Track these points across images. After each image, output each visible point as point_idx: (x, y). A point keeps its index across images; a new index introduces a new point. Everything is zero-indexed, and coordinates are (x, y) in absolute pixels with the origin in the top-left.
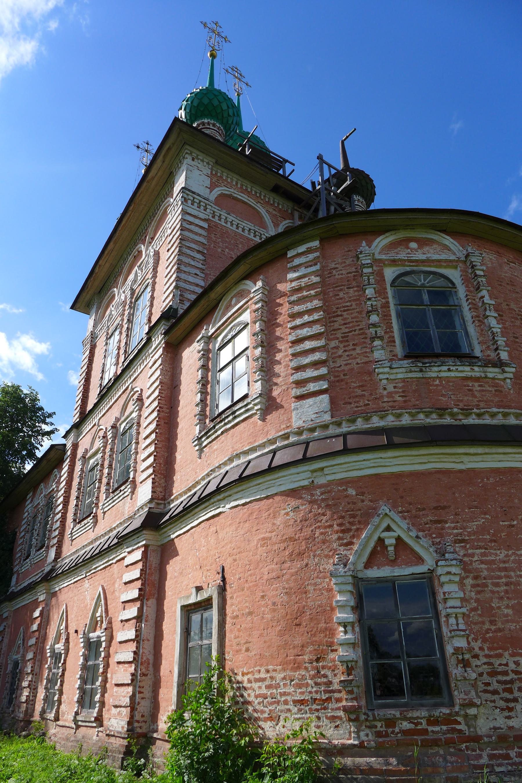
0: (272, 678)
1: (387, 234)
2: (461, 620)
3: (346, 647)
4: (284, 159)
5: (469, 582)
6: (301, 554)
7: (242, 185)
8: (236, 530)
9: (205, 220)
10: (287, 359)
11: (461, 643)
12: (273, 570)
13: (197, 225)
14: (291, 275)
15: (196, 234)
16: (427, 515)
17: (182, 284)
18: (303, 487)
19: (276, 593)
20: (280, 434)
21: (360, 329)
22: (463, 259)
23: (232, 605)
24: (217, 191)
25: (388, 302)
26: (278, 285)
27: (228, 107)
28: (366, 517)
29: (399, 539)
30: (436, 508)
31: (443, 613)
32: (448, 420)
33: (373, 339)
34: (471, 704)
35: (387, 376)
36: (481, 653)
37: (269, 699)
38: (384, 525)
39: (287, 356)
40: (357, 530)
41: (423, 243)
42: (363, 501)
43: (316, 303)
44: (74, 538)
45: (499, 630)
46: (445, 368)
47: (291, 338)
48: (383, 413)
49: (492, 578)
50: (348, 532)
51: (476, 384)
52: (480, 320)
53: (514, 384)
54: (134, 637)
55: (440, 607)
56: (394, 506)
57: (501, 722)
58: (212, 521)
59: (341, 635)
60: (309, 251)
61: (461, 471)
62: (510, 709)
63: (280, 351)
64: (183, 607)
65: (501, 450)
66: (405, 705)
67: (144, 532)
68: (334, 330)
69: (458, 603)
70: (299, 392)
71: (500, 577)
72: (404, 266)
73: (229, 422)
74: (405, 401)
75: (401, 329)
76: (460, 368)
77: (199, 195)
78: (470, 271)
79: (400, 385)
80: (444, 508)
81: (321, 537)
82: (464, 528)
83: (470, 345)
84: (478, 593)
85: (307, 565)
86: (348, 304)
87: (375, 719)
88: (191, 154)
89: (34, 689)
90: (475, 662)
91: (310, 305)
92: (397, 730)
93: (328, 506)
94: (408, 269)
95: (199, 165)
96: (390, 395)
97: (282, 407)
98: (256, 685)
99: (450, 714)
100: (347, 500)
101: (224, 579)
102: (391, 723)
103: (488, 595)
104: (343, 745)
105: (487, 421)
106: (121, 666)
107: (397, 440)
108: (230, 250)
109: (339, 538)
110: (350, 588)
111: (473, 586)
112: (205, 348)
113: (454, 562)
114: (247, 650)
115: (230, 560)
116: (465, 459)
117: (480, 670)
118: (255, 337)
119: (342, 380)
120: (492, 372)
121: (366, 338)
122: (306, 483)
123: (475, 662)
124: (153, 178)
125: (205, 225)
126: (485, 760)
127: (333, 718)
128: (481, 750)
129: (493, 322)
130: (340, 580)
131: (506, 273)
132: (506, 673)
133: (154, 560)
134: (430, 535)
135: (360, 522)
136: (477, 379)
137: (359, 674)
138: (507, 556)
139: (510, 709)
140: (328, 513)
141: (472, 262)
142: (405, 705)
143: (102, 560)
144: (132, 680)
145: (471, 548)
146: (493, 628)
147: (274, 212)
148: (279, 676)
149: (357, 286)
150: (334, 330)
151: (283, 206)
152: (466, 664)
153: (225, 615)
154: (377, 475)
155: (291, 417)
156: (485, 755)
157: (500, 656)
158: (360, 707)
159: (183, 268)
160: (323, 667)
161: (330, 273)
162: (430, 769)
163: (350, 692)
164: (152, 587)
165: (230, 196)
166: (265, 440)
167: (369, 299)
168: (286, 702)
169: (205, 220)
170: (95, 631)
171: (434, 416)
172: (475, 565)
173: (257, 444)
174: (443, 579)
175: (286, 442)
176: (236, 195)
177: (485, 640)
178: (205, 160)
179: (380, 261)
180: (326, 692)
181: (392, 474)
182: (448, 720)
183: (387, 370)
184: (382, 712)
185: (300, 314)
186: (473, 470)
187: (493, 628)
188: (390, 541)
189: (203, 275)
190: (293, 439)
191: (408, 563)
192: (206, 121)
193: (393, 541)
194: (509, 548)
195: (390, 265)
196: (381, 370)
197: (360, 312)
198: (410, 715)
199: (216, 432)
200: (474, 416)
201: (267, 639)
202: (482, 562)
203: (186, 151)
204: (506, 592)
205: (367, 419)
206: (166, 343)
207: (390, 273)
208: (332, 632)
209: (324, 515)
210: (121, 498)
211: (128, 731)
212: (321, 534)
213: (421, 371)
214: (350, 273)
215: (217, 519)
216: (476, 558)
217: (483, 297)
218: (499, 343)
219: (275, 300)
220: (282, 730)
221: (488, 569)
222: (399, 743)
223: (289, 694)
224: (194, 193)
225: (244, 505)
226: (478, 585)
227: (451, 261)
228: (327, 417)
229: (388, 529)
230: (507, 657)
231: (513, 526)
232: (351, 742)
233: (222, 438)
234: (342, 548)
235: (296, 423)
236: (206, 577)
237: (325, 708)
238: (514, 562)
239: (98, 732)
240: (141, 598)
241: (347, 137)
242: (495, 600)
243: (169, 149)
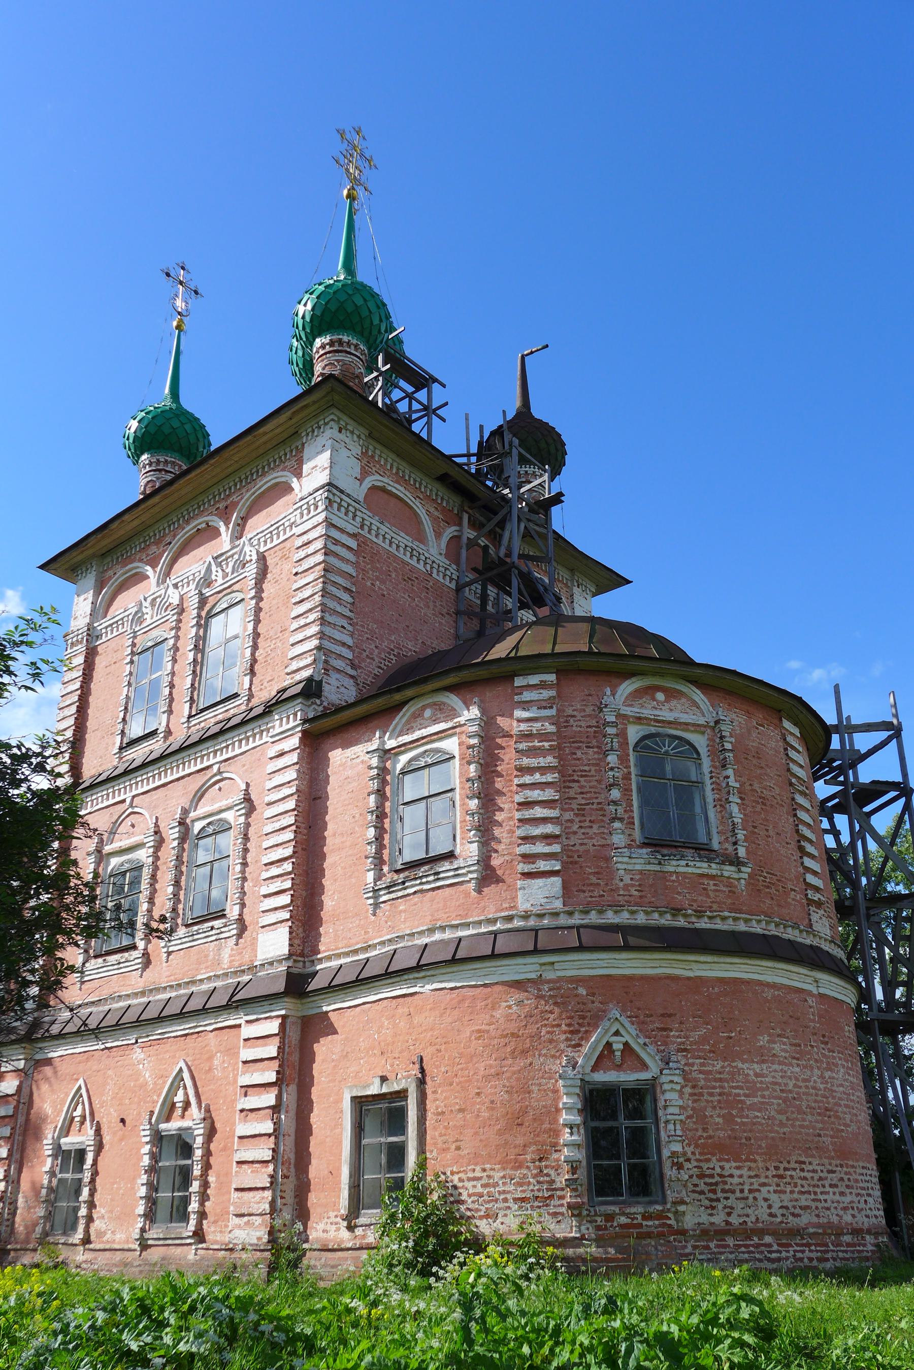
0: (489, 1177)
1: (633, 679)
2: (678, 1127)
3: (571, 1148)
4: (431, 377)
5: (688, 1090)
6: (524, 1052)
7: (398, 469)
8: (441, 1016)
9: (354, 536)
10: (511, 823)
11: (677, 1147)
12: (491, 1066)
13: (344, 545)
14: (519, 713)
15: (342, 559)
16: (654, 1022)
17: (327, 644)
18: (529, 980)
19: (496, 1091)
20: (503, 914)
21: (599, 803)
22: (712, 724)
23: (436, 1100)
24: (368, 482)
25: (630, 773)
26: (499, 718)
27: (365, 300)
28: (595, 1019)
29: (626, 1044)
30: (663, 1015)
31: (663, 1119)
32: (681, 922)
33: (613, 820)
34: (683, 1202)
35: (625, 866)
36: (693, 1158)
37: (486, 1198)
38: (613, 1030)
39: (511, 818)
40: (586, 1032)
41: (672, 694)
42: (593, 1002)
43: (550, 760)
44: (86, 979)
45: (710, 1137)
46: (683, 863)
47: (519, 798)
48: (617, 907)
49: (708, 1087)
50: (577, 1035)
51: (712, 883)
52: (722, 804)
53: (748, 884)
54: (271, 1131)
55: (660, 1113)
56: (623, 1011)
57: (705, 1218)
58: (401, 1000)
59: (566, 1136)
60: (543, 685)
61: (689, 978)
62: (713, 1208)
63: (501, 809)
64: (354, 1099)
65: (729, 960)
66: (623, 1202)
67: (286, 999)
68: (569, 798)
69: (677, 1111)
70: (527, 868)
71: (714, 1088)
72: (649, 725)
73: (428, 882)
74: (641, 897)
75: (641, 807)
76: (698, 864)
77: (348, 496)
78: (718, 740)
79: (637, 877)
80: (670, 1015)
81: (548, 1036)
82: (687, 1037)
83: (709, 833)
84: (695, 1101)
85: (531, 1064)
86: (586, 768)
87: (596, 1215)
88: (338, 422)
89: (10, 1204)
90: (687, 1165)
91: (542, 762)
92: (615, 1224)
93: (556, 1004)
94: (653, 730)
95: (347, 440)
96: (626, 887)
97: (503, 881)
98: (469, 1184)
99: (662, 1211)
100: (577, 999)
101: (422, 1071)
102: (610, 1217)
103: (703, 1104)
104: (565, 1237)
105: (719, 925)
106: (245, 1166)
107: (632, 941)
108: (383, 582)
109: (567, 1039)
110: (577, 1091)
111: (691, 1095)
112: (381, 765)
113: (677, 1072)
114: (458, 1148)
115: (431, 1050)
116: (695, 966)
117: (691, 1172)
118: (469, 784)
119: (576, 863)
121: (604, 815)
122: (533, 976)
123: (687, 1165)
124: (265, 433)
125: (353, 544)
126: (689, 1250)
127: (555, 1214)
128: (686, 1241)
129: (735, 809)
130: (569, 1082)
131: (754, 741)
132: (712, 1176)
133: (294, 1034)
134: (656, 1043)
135: (589, 1024)
136: (712, 877)
137: (582, 1174)
138: (723, 1067)
139: (713, 1208)
140: (557, 1010)
141: (721, 731)
142: (623, 1202)
143: (180, 1024)
144: (272, 1183)
145: (692, 1057)
146: (705, 1135)
147: (436, 513)
148: (497, 1175)
149: (598, 747)
150: (569, 798)
151: (448, 502)
152: (680, 1167)
153: (425, 1110)
154: (608, 976)
155: (516, 896)
156: (689, 1245)
157: (708, 1160)
158: (583, 1203)
159: (328, 618)
160: (546, 1167)
161: (567, 722)
162: (644, 1257)
163: (575, 1190)
164: (295, 1070)
165: (383, 490)
166: (482, 918)
167: (612, 769)
168: (505, 1200)
169: (354, 536)
170: (168, 1119)
171: (668, 916)
172: (694, 1075)
173: (471, 920)
174: (666, 1087)
175: (510, 926)
176: (390, 488)
177: (697, 1146)
178: (356, 432)
179: (625, 717)
180: (548, 1190)
181: (624, 976)
182: (660, 1216)
183: (626, 859)
184: (603, 1208)
185: (530, 770)
186: (700, 978)
187: (705, 1135)
188: (618, 1047)
189: (351, 628)
190: (517, 923)
191: (634, 1069)
192: (345, 338)
193: (621, 1047)
194: (725, 1059)
195: (634, 723)
196: (620, 859)
197: (599, 782)
198: (628, 1211)
199: (405, 889)
200: (706, 920)
201: (483, 1137)
202: (701, 1072)
203: (332, 417)
204: (719, 1102)
205: (601, 912)
206: (304, 732)
207: (634, 733)
208: (557, 1133)
209: (551, 1012)
210: (214, 938)
211: (269, 1242)
212: (548, 1032)
213: (660, 864)
214: (590, 727)
215: (409, 999)
216: (695, 1068)
217: (728, 777)
218: (739, 836)
219: (494, 738)
220: (501, 1227)
221: (705, 1079)
222: (617, 1236)
223: (509, 1192)
224: (342, 492)
225: (452, 989)
226: (695, 1094)
227: (699, 725)
228: (558, 904)
229: (617, 1033)
230: (714, 1163)
231: (731, 1038)
232: (573, 1235)
233: (416, 898)
234: (570, 1049)
235: (523, 905)
236: (392, 1066)
237: (547, 1205)
238: (728, 1073)
239: (196, 1249)
240: (278, 1083)
241: (532, 353)
242: (709, 1109)
243: (306, 406)
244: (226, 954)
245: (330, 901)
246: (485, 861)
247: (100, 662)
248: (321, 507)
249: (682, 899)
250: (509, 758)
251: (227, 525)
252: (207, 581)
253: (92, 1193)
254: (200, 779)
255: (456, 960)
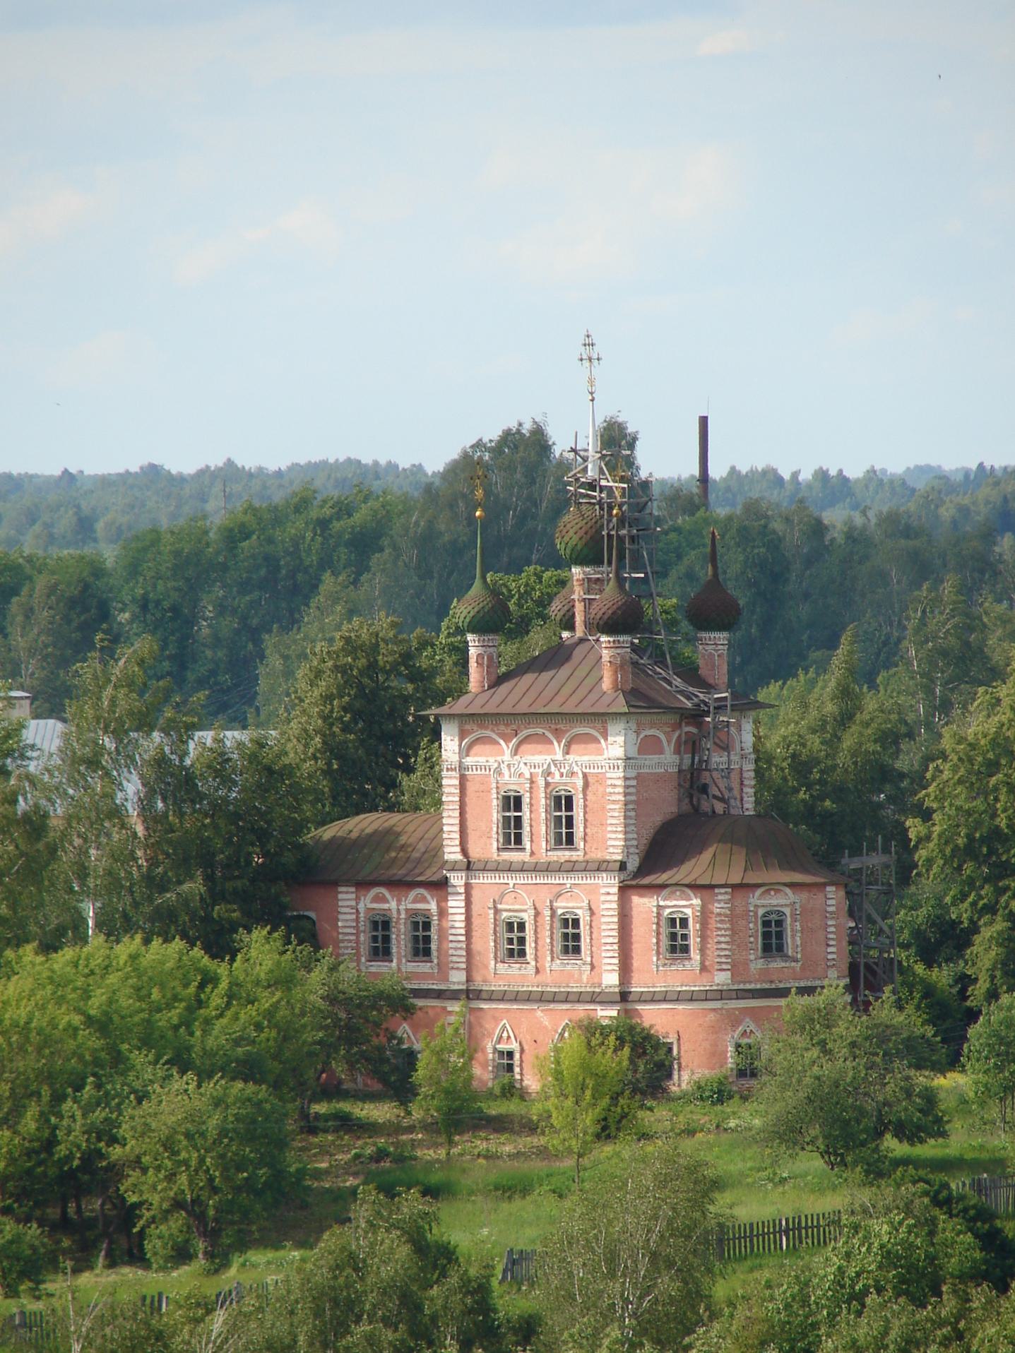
32: (773, 986)
48: (750, 982)
52: (793, 936)
120: (793, 964)
207: (761, 912)
235: (717, 981)
244: (585, 978)
245: (636, 963)
246: (702, 963)
247: (471, 788)
248: (621, 770)
249: (774, 978)
250: (713, 923)
251: (559, 742)
252: (548, 773)
253: (522, 1070)
254: (558, 889)
255: (692, 998)
